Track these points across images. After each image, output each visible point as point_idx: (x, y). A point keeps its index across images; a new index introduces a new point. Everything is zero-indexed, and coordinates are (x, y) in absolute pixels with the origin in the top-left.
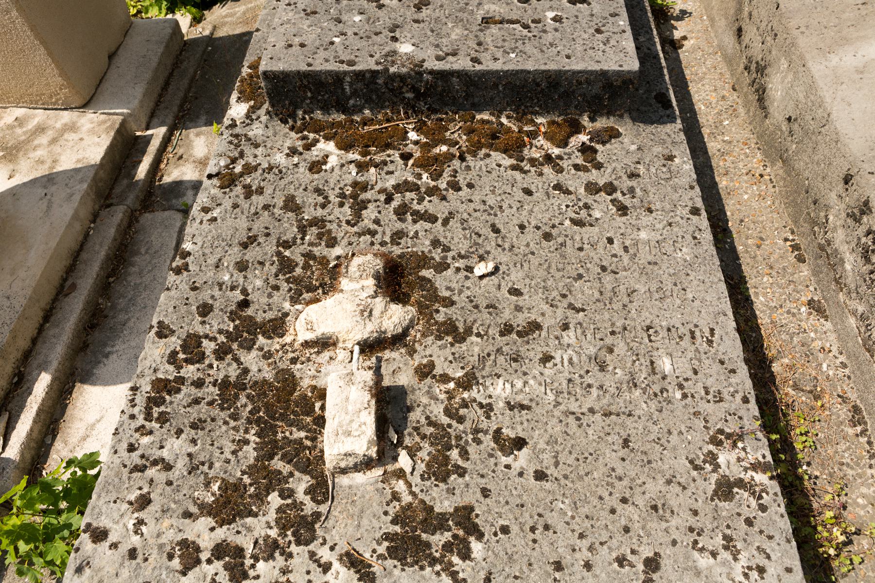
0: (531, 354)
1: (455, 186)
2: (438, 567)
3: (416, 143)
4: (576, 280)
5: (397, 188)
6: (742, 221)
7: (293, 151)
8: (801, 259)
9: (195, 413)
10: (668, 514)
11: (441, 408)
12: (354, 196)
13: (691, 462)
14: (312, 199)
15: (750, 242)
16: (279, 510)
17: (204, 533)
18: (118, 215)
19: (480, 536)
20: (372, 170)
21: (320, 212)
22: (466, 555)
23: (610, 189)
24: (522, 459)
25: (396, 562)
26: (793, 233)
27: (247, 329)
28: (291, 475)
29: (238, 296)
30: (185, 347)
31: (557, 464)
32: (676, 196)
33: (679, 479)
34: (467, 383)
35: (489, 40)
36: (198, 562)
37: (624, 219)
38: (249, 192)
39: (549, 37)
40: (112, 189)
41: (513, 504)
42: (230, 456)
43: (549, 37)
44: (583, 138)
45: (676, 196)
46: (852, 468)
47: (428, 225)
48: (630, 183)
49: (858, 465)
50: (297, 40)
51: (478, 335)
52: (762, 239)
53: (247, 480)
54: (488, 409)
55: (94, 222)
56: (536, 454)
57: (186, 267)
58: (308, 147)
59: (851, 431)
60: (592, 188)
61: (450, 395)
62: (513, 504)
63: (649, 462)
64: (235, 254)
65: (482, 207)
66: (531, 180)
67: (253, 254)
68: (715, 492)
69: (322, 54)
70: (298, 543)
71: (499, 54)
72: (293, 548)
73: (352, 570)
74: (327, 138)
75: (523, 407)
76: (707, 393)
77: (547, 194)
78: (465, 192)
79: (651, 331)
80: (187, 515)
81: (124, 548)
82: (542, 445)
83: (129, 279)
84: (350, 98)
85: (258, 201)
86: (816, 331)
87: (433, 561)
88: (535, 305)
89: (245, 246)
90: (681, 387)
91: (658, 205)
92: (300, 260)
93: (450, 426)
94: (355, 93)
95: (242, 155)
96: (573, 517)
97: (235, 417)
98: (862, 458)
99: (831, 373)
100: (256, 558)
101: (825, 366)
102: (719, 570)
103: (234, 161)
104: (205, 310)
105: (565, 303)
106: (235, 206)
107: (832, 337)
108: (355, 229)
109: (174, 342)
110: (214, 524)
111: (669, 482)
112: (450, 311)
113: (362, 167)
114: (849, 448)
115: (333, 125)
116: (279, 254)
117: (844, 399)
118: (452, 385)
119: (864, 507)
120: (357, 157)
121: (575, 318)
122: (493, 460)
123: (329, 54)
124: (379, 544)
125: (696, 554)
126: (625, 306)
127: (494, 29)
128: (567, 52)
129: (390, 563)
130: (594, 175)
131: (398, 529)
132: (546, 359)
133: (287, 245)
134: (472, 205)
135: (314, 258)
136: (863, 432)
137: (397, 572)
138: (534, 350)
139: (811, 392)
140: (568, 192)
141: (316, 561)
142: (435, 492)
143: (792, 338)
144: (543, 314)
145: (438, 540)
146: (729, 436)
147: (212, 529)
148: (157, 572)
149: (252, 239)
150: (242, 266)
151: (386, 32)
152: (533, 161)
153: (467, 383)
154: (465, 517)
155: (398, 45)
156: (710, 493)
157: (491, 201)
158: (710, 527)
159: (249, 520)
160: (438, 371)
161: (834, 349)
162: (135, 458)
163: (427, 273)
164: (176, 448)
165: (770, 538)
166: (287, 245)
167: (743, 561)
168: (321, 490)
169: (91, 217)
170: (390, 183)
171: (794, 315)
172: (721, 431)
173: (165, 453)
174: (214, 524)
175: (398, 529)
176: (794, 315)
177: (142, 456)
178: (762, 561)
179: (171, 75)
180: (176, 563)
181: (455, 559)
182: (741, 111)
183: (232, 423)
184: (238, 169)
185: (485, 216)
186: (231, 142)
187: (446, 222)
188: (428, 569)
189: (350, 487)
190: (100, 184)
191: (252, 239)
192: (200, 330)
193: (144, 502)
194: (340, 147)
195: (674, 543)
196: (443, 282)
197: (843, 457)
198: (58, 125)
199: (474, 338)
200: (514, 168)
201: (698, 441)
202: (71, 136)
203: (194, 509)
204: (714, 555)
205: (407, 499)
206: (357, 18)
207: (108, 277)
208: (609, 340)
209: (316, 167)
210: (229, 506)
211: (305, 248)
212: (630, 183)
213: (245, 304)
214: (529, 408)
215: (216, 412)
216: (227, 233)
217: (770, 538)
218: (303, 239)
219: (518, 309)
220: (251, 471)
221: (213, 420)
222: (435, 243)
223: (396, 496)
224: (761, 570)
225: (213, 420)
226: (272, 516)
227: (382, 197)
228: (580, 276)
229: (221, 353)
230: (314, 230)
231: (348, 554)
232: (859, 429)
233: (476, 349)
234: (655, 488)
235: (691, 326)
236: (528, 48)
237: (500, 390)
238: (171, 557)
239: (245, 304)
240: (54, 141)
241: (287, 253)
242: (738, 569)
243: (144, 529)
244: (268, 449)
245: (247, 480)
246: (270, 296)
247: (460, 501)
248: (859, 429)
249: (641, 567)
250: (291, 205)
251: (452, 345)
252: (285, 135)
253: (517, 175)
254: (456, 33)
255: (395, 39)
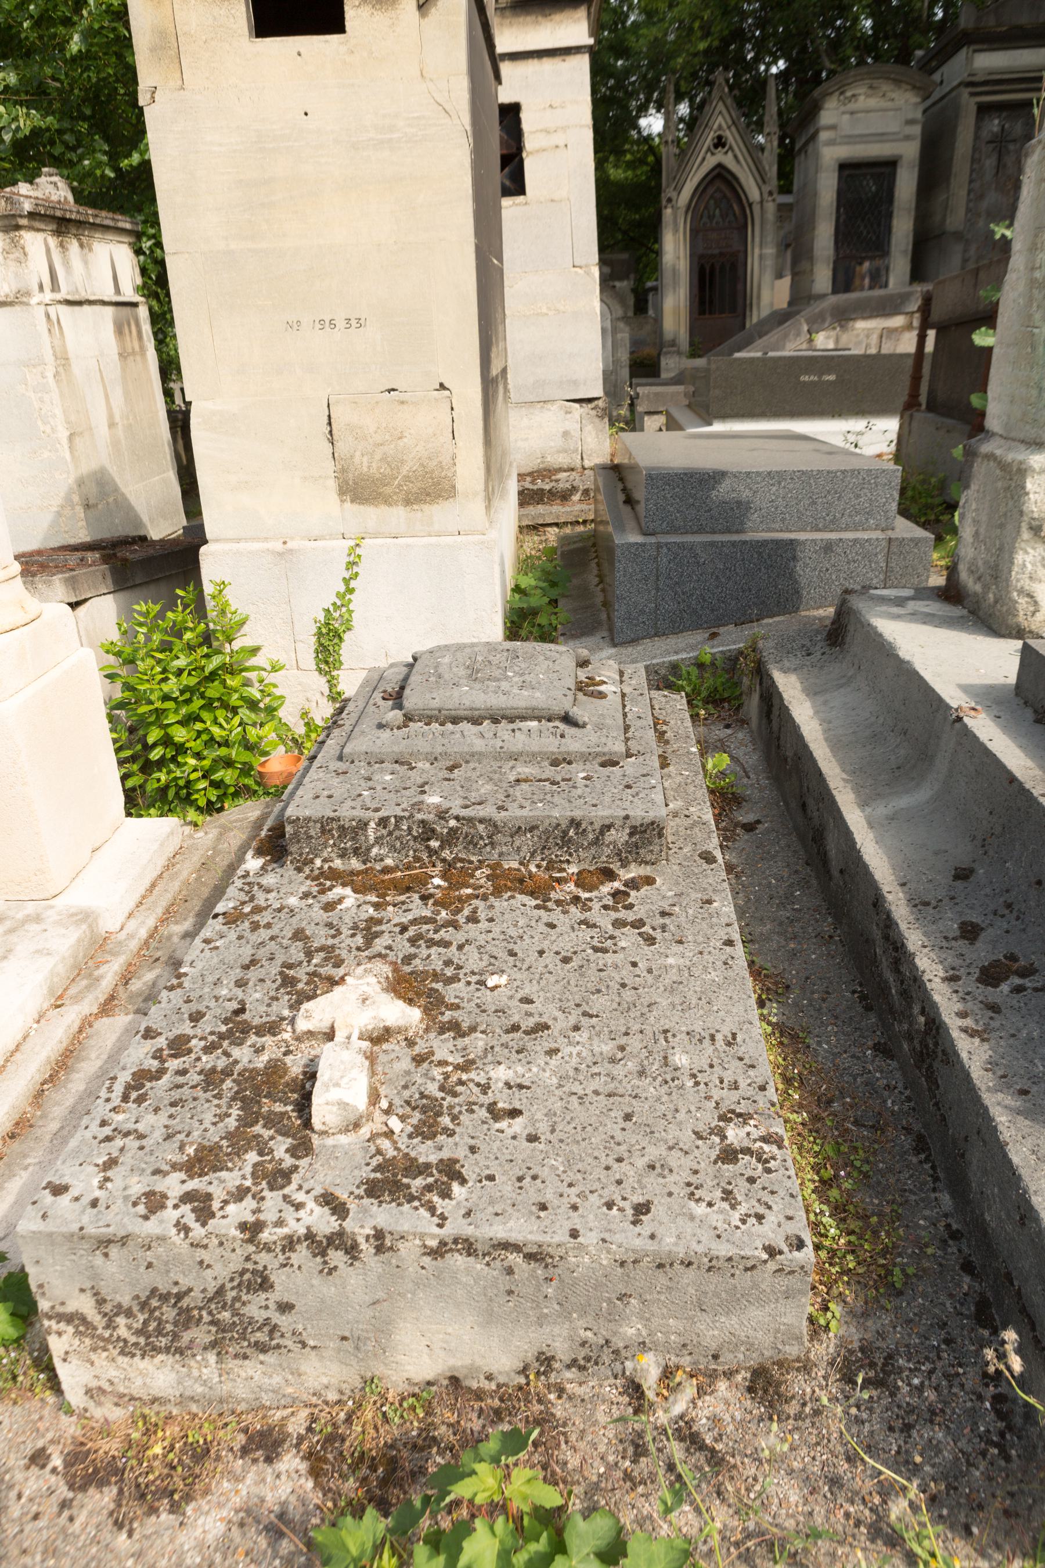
0: (539, 1048)
1: (473, 919)
2: (416, 1203)
3: (438, 887)
4: (593, 993)
5: (414, 922)
6: (807, 978)
7: (306, 895)
8: (868, 1008)
9: (176, 1094)
10: (666, 1172)
11: (436, 1085)
12: (368, 929)
13: (696, 1133)
14: (323, 931)
15: (816, 996)
16: (255, 1165)
17: (174, 1185)
18: (72, 1016)
19: (463, 1181)
20: (390, 908)
21: (330, 942)
22: (446, 1194)
23: (638, 924)
24: (518, 1125)
25: (373, 1200)
26: (861, 985)
27: (238, 1027)
28: (272, 1138)
29: (235, 1005)
30: (170, 1046)
31: (553, 1131)
32: (710, 932)
33: (681, 1145)
34: (466, 1066)
35: (518, 794)
36: (163, 1207)
37: (652, 948)
38: (255, 927)
39: (579, 792)
40: (66, 990)
41: (502, 1158)
42: (209, 1126)
43: (579, 792)
44: (616, 884)
45: (710, 932)
46: (915, 1194)
47: (441, 950)
48: (662, 921)
49: (921, 1190)
50: (326, 793)
51: (483, 1032)
52: (828, 993)
53: (224, 1143)
54: (485, 1088)
55: (38, 1022)
56: (533, 1122)
57: (180, 985)
58: (322, 892)
59: (915, 1160)
60: (618, 924)
61: (447, 1076)
62: (502, 1158)
63: (652, 1132)
64: (238, 973)
65: (502, 937)
66: (556, 916)
67: (253, 975)
68: (718, 1158)
69: (349, 803)
70: (272, 1189)
71: (527, 804)
72: (266, 1193)
73: (326, 1208)
74: (344, 885)
75: (521, 1087)
76: (722, 1082)
77: (573, 928)
78: (484, 925)
79: (669, 1035)
80: (157, 1172)
81: (86, 1200)
82: (539, 1116)
83: (70, 1086)
84: (373, 845)
85: (264, 934)
86: (881, 1072)
87: (411, 1199)
88: (545, 1009)
89: (246, 967)
90: (694, 1076)
91: (690, 938)
92: (305, 978)
93: (443, 1099)
94: (378, 841)
95: (252, 899)
96: (564, 1172)
97: (218, 1096)
98: (925, 1183)
99: (896, 1108)
100: (226, 1202)
101: (889, 1102)
102: (715, 1217)
103: (243, 903)
104: (196, 1018)
105: (580, 1011)
106: (240, 938)
107: (898, 1075)
108: (366, 953)
109: (161, 1042)
110: (185, 1177)
111: (671, 1148)
112: (456, 1014)
113: (377, 906)
114: (911, 1176)
115: (352, 873)
116: (281, 973)
117: (907, 1130)
118: (450, 1068)
119: (925, 1228)
120: (375, 899)
121: (585, 1021)
122: (486, 1126)
123: (358, 803)
124: (358, 1187)
125: (692, 1204)
126: (642, 1014)
127: (524, 786)
128: (594, 802)
129: (366, 1201)
130: (623, 914)
131: (378, 1175)
132: (552, 1052)
133: (290, 966)
134: (491, 935)
135: (319, 976)
136: (927, 1160)
137: (375, 1208)
138: (539, 1045)
139: (873, 1127)
140: (594, 926)
141: (289, 1202)
142: (422, 1148)
143: (855, 1080)
144: (555, 1019)
145: (418, 1183)
146: (740, 1115)
147: (183, 1182)
148: (119, 1217)
149: (253, 962)
150: (241, 984)
151: (414, 788)
152: (558, 903)
153: (466, 1066)
154: (451, 1171)
155: (425, 797)
156: (713, 1157)
157: (512, 932)
158: (711, 1184)
159: (224, 1174)
160: (437, 1057)
161: (900, 1085)
162: (107, 1131)
163: (439, 986)
164: (153, 1123)
165: (772, 1193)
166: (290, 966)
167: (743, 1209)
168: (302, 1148)
169: (36, 1017)
170: (406, 919)
171: (858, 1058)
172: (733, 1112)
173: (141, 1127)
174: (185, 1177)
175: (378, 1175)
176: (858, 1058)
177: (115, 1130)
178: (761, 1210)
179: (160, 876)
180: (141, 1209)
181: (436, 1199)
182: (814, 882)
183: (216, 1102)
184: (247, 909)
185: (505, 944)
186: (241, 890)
187: (460, 947)
188: (407, 1206)
189: (334, 1146)
190: (55, 980)
191: (253, 962)
192: (190, 1032)
193: (112, 1163)
194: (355, 891)
195: (670, 1194)
196: (451, 993)
197: (906, 1184)
198: (20, 916)
199: (478, 1035)
200: (537, 907)
201: (708, 1118)
202: (34, 928)
203: (166, 1168)
204: (710, 1205)
205: (391, 1153)
206: (388, 778)
207: (42, 1084)
208: (623, 1040)
209: (329, 907)
210: (205, 1161)
211: (311, 969)
212: (662, 921)
213: (242, 1010)
214: (528, 1088)
215: (199, 1093)
216: (230, 958)
217: (772, 1193)
218: (309, 962)
219: (529, 1014)
220: (229, 1136)
221: (195, 1099)
222: (448, 963)
223: (379, 1152)
224: (760, 1218)
225: (195, 1099)
226: (248, 1169)
227: (398, 929)
228: (599, 991)
229: (208, 1049)
230: (322, 954)
231: (323, 1195)
232: (923, 1156)
233: (481, 1043)
234: (654, 1152)
235: (713, 1031)
236: (557, 799)
237: (501, 1074)
238: (135, 1204)
239: (242, 1010)
240: (11, 931)
241: (291, 972)
242: (735, 1217)
243: (109, 1185)
244: (248, 1120)
245: (224, 1143)
246: (269, 1005)
247: (445, 1154)
248: (923, 1156)
249: (630, 1212)
250: (299, 935)
251: (454, 1038)
252: (301, 883)
253: (542, 912)
254: (485, 789)
255: (424, 792)
